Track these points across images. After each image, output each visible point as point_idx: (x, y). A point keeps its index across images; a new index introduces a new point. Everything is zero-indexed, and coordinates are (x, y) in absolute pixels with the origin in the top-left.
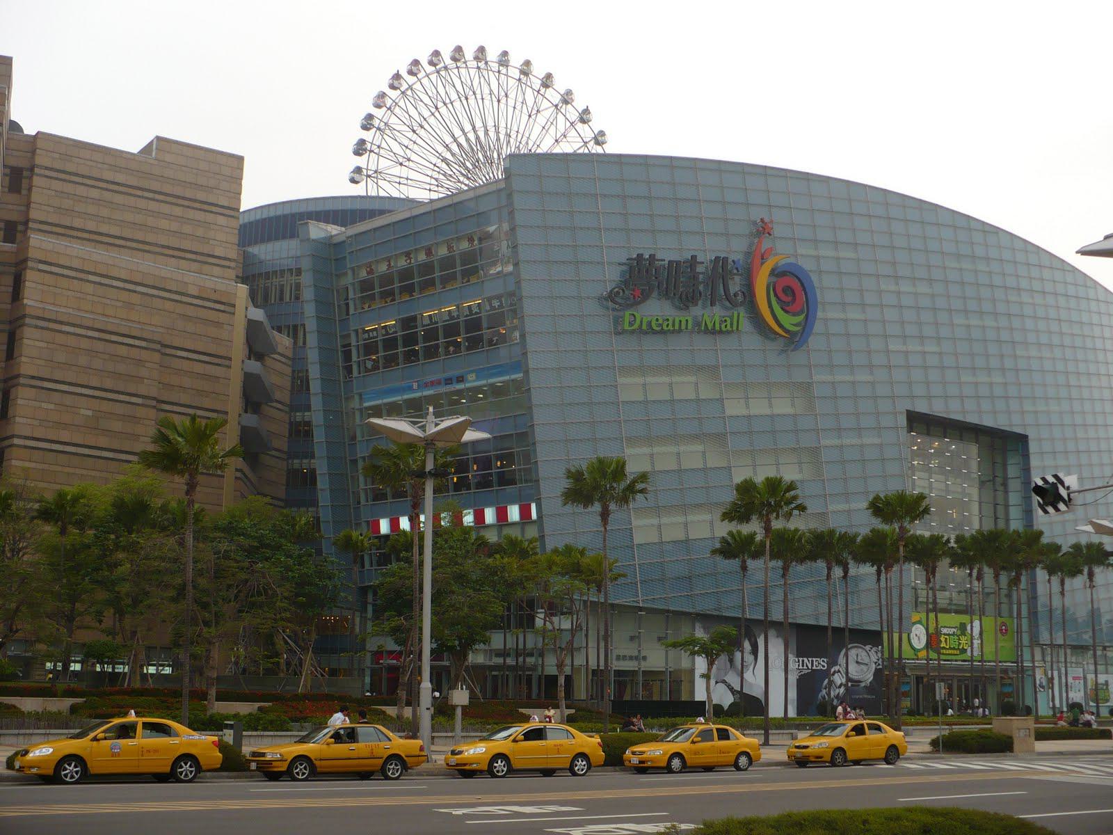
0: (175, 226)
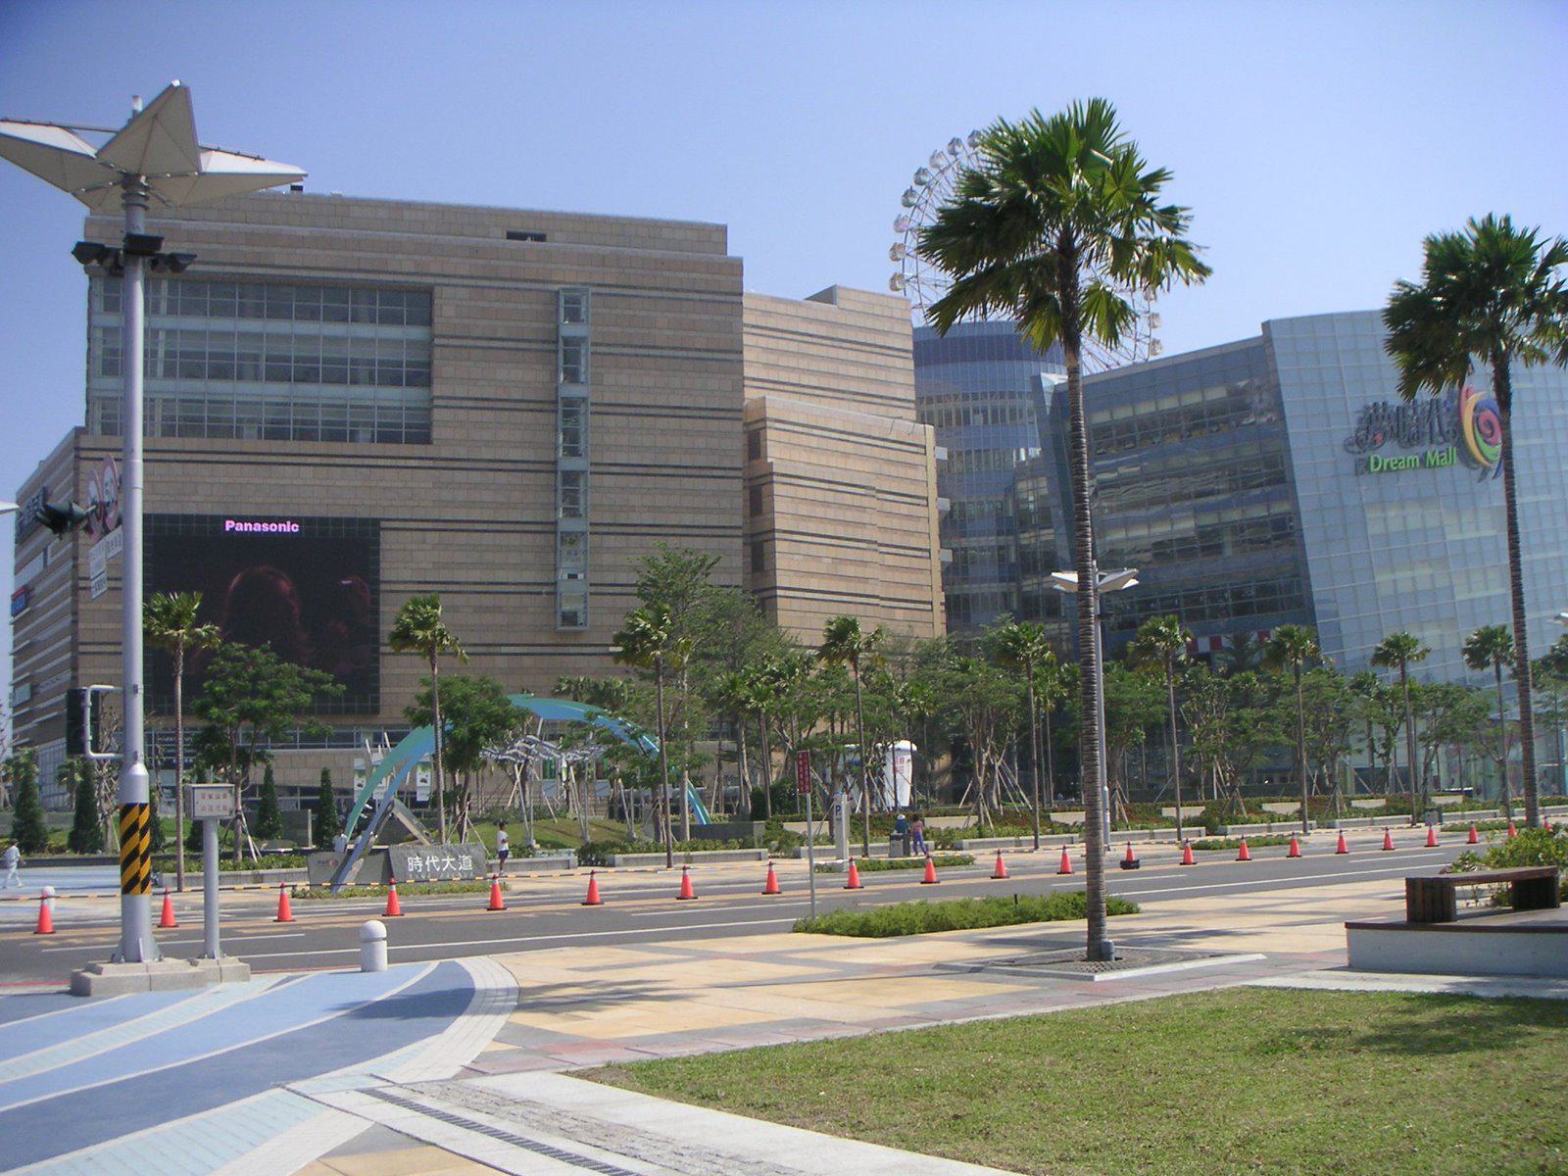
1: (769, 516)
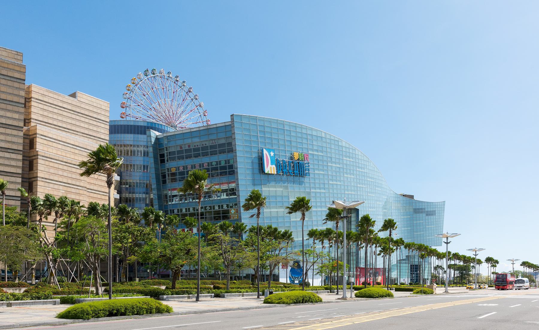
1: (36, 171)
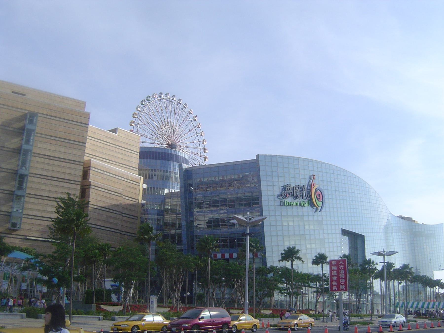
0: (122, 157)
1: (88, 199)
